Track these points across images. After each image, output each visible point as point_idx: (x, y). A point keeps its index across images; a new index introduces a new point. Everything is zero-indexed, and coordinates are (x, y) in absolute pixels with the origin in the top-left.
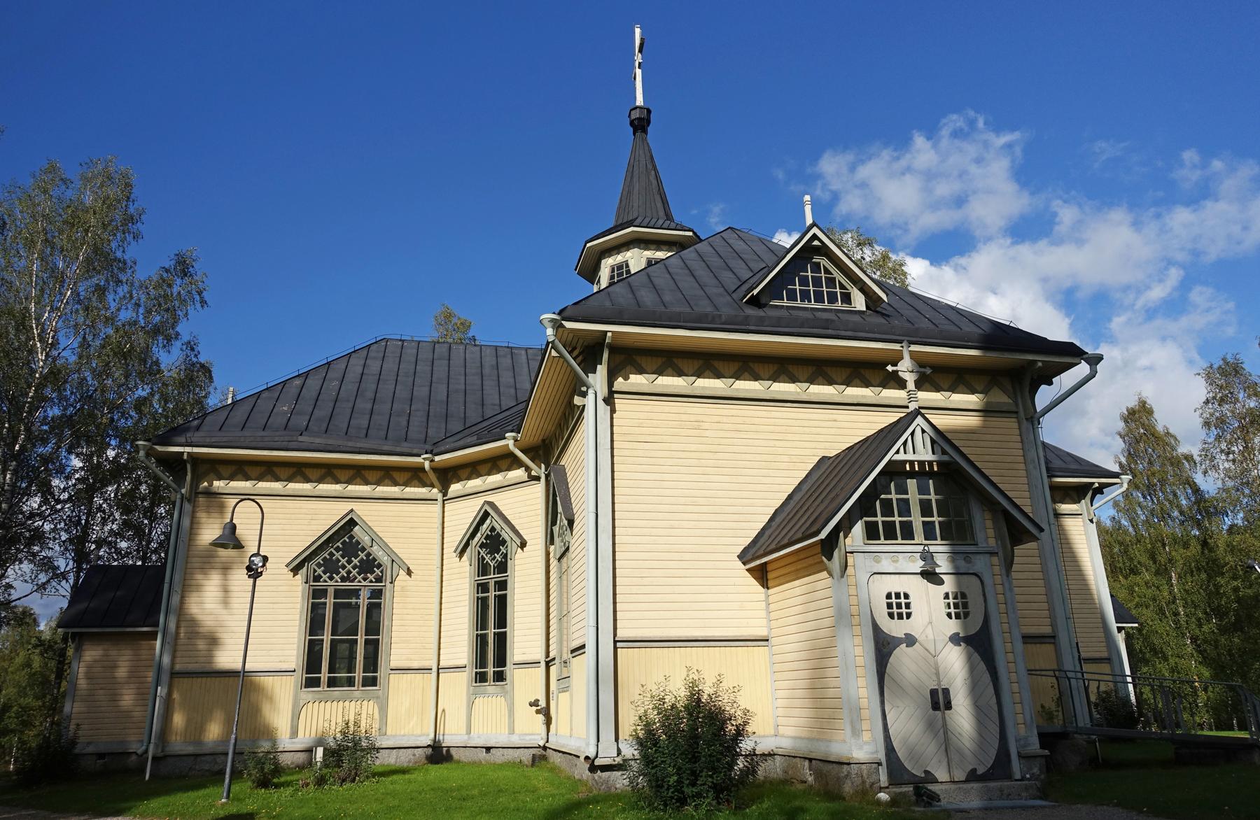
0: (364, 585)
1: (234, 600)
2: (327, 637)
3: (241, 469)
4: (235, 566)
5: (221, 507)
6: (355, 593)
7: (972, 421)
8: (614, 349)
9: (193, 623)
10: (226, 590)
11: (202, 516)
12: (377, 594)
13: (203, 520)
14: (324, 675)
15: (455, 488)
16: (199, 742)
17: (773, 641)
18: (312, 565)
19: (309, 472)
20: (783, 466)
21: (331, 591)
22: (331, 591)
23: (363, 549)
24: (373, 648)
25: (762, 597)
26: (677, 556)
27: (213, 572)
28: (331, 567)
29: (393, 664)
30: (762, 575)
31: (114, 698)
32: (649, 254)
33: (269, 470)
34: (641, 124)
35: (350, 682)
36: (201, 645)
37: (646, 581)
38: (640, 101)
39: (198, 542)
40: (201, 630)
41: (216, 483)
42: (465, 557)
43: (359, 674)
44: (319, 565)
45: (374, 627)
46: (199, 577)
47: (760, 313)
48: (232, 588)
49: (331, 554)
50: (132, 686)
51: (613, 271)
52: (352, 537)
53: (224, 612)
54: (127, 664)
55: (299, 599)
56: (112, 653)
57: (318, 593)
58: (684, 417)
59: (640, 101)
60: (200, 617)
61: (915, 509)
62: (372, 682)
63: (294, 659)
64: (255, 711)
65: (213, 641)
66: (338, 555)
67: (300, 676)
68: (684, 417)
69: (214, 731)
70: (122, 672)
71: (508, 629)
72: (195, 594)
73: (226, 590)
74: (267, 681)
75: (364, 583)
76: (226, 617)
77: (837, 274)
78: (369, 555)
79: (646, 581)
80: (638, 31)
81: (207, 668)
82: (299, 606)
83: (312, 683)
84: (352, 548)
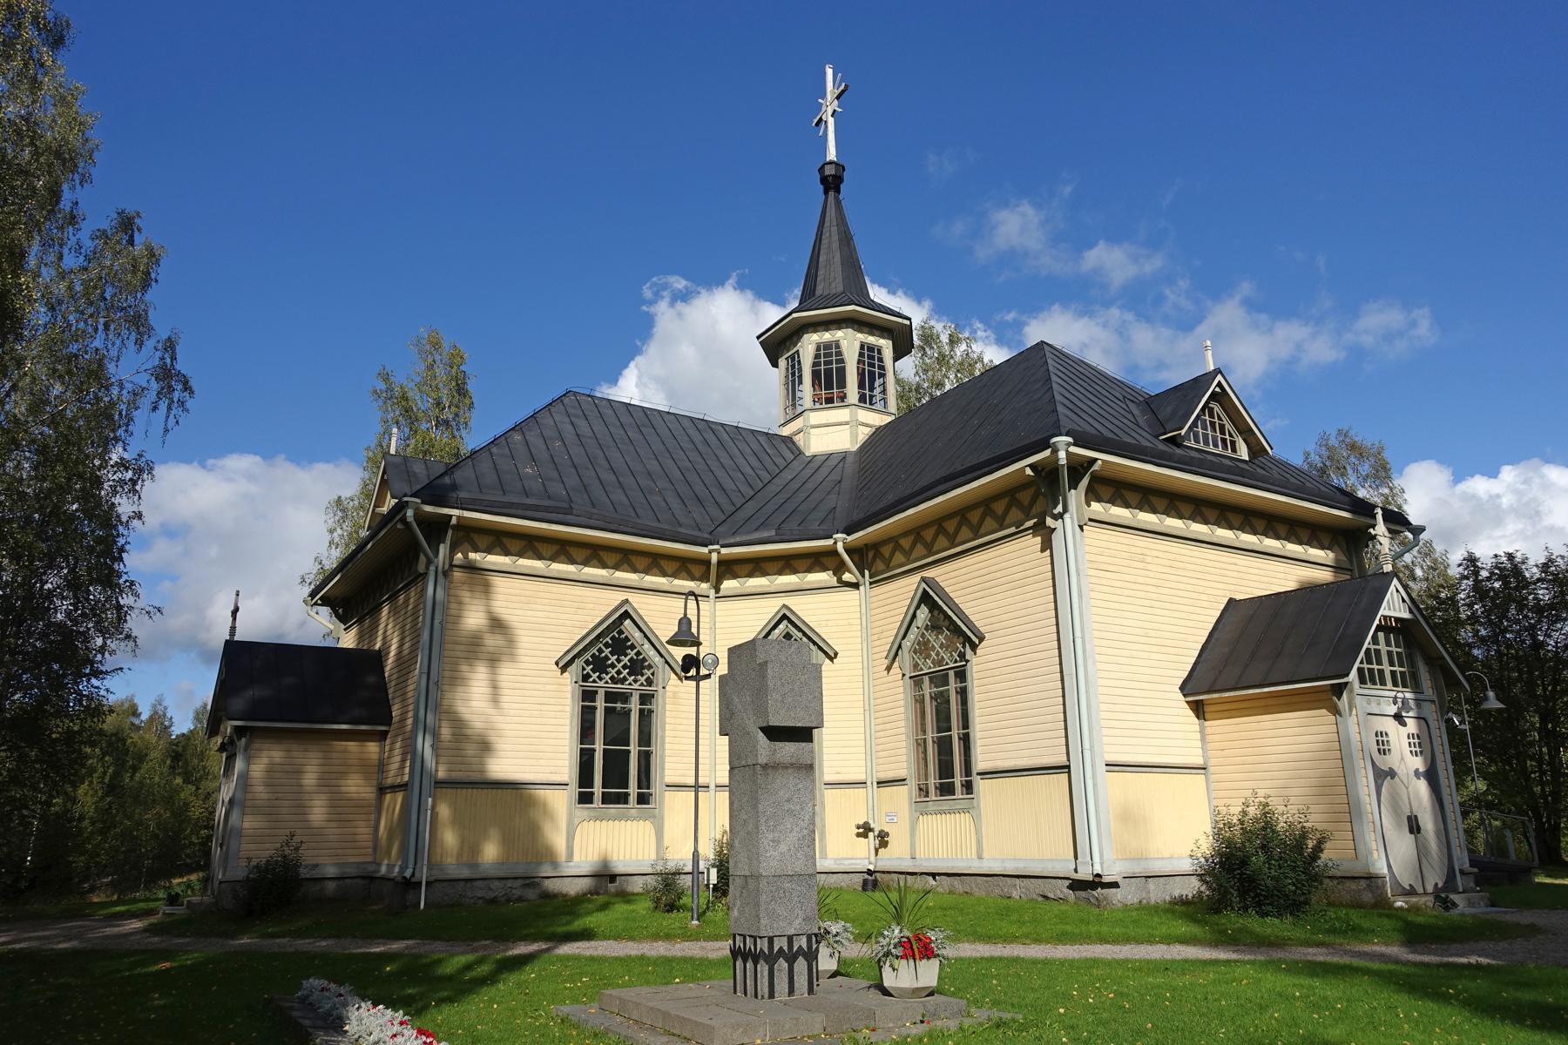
0: (634, 686)
1: (504, 699)
2: (599, 747)
3: (500, 540)
4: (504, 658)
5: (486, 589)
6: (625, 698)
7: (1325, 576)
8: (1097, 480)
9: (458, 724)
10: (495, 687)
11: (465, 595)
12: (646, 699)
13: (467, 600)
14: (598, 789)
15: (729, 585)
16: (474, 866)
17: (1211, 769)
18: (579, 663)
19: (574, 552)
20: (1205, 604)
21: (601, 693)
22: (601, 693)
23: (633, 647)
24: (645, 759)
25: (1197, 728)
26: (1137, 685)
27: (479, 663)
28: (600, 665)
29: (668, 780)
30: (1199, 709)
31: (301, 809)
32: (861, 337)
33: (530, 545)
34: (832, 182)
35: (623, 799)
36: (471, 750)
37: (1117, 708)
38: (832, 155)
39: (462, 627)
40: (469, 732)
41: (472, 555)
42: (896, 669)
43: (633, 789)
44: (587, 663)
45: (646, 738)
46: (464, 668)
47: (1178, 451)
48: (503, 684)
49: (600, 651)
50: (323, 796)
51: (818, 349)
52: (621, 632)
53: (492, 711)
54: (314, 769)
55: (569, 701)
56: (295, 754)
57: (588, 695)
58: (1133, 549)
59: (832, 155)
60: (467, 717)
61: (1385, 659)
62: (643, 799)
63: (566, 770)
64: (534, 831)
65: (485, 747)
66: (607, 651)
67: (574, 790)
68: (1133, 549)
69: (491, 852)
70: (310, 779)
71: (653, 748)
72: (460, 689)
73: (495, 687)
74: (543, 793)
75: (636, 686)
76: (495, 719)
77: (1228, 426)
78: (638, 653)
79: (1117, 708)
80: (829, 72)
81: (474, 777)
82: (568, 709)
83: (585, 798)
84: (621, 645)
